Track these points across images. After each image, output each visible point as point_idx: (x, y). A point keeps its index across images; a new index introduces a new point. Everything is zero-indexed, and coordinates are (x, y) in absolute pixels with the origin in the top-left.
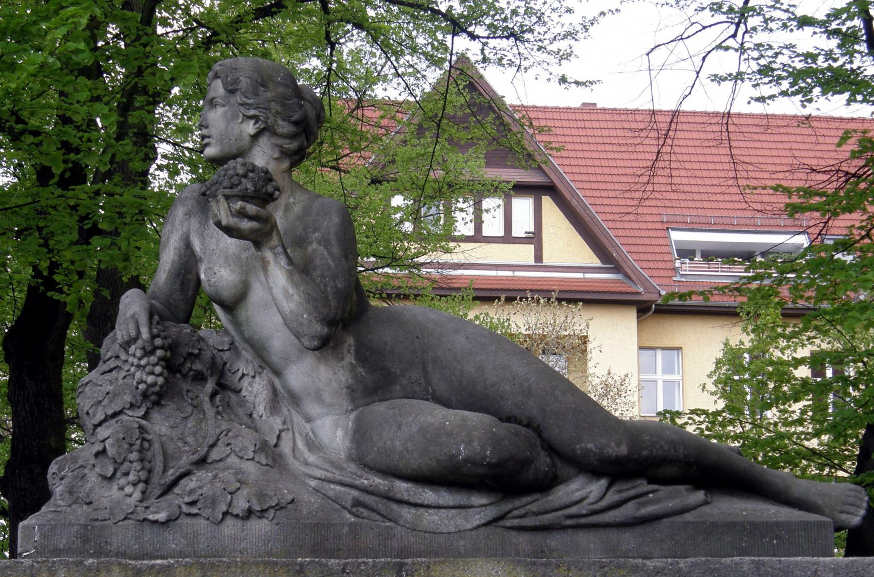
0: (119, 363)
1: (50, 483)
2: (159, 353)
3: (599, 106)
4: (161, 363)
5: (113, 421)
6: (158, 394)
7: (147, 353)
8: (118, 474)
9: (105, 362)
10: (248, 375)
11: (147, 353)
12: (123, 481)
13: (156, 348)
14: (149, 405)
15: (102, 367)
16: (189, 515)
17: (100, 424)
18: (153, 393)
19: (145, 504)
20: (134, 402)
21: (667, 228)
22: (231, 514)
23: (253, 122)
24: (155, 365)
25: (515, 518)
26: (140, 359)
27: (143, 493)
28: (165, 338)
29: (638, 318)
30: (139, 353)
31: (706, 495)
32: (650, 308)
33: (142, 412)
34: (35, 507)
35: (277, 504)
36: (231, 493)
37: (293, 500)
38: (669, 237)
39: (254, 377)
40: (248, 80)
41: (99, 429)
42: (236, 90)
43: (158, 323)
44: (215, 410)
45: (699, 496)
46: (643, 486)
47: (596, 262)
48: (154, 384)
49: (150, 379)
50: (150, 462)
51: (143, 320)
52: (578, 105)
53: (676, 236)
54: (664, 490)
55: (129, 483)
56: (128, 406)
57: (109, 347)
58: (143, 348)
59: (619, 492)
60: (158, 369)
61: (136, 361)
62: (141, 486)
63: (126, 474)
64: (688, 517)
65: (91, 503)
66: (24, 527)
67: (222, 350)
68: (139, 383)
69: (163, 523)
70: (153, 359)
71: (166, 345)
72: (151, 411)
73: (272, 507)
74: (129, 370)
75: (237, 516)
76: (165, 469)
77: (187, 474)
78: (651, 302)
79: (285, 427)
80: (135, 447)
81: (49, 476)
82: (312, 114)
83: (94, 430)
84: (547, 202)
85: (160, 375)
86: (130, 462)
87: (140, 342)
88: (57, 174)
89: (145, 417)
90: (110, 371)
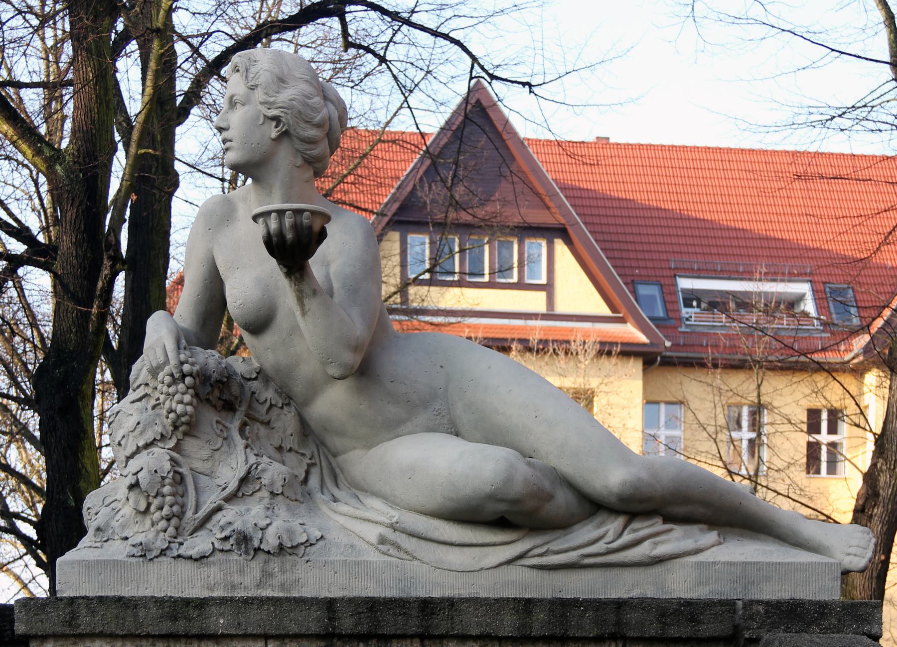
0: (149, 390)
1: (85, 518)
2: (188, 380)
3: (612, 141)
4: (191, 391)
5: (145, 452)
6: (188, 424)
7: (174, 381)
8: (152, 508)
9: (134, 390)
10: (275, 406)
11: (174, 381)
12: (157, 515)
13: (184, 376)
14: (180, 436)
15: (132, 395)
16: (222, 551)
17: (132, 456)
18: (183, 423)
19: (180, 540)
20: (164, 433)
21: (675, 276)
22: (263, 550)
23: (274, 124)
24: (183, 394)
25: (534, 556)
26: (169, 386)
27: (177, 528)
28: (193, 364)
29: (644, 370)
30: (168, 379)
31: (719, 535)
32: (656, 360)
33: (172, 444)
34: (72, 544)
35: (307, 541)
36: (261, 529)
37: (322, 537)
38: (676, 285)
39: (282, 408)
40: (267, 74)
41: (131, 462)
42: (257, 86)
43: (185, 348)
44: (244, 441)
45: (712, 536)
46: (658, 525)
47: (605, 311)
48: (185, 414)
49: (180, 408)
50: (182, 496)
51: (170, 346)
52: (591, 138)
53: (685, 283)
54: (678, 530)
55: (162, 518)
56: (158, 437)
57: (139, 370)
58: (172, 375)
59: (635, 531)
60: (187, 398)
61: (165, 389)
62: (174, 521)
63: (161, 508)
64: (700, 557)
65: (127, 538)
66: (61, 562)
67: (250, 379)
68: (169, 413)
69: (196, 560)
70: (181, 387)
71: (194, 372)
72: (182, 442)
73: (302, 544)
74: (158, 399)
75: (269, 552)
76: (196, 512)
77: (219, 509)
78: (656, 354)
79: (313, 461)
80: (167, 481)
81: (84, 511)
82: (335, 115)
83: (127, 462)
84: (560, 247)
85: (190, 404)
86: (163, 496)
87: (167, 369)
88: (76, 183)
89: (177, 448)
90: (140, 400)
